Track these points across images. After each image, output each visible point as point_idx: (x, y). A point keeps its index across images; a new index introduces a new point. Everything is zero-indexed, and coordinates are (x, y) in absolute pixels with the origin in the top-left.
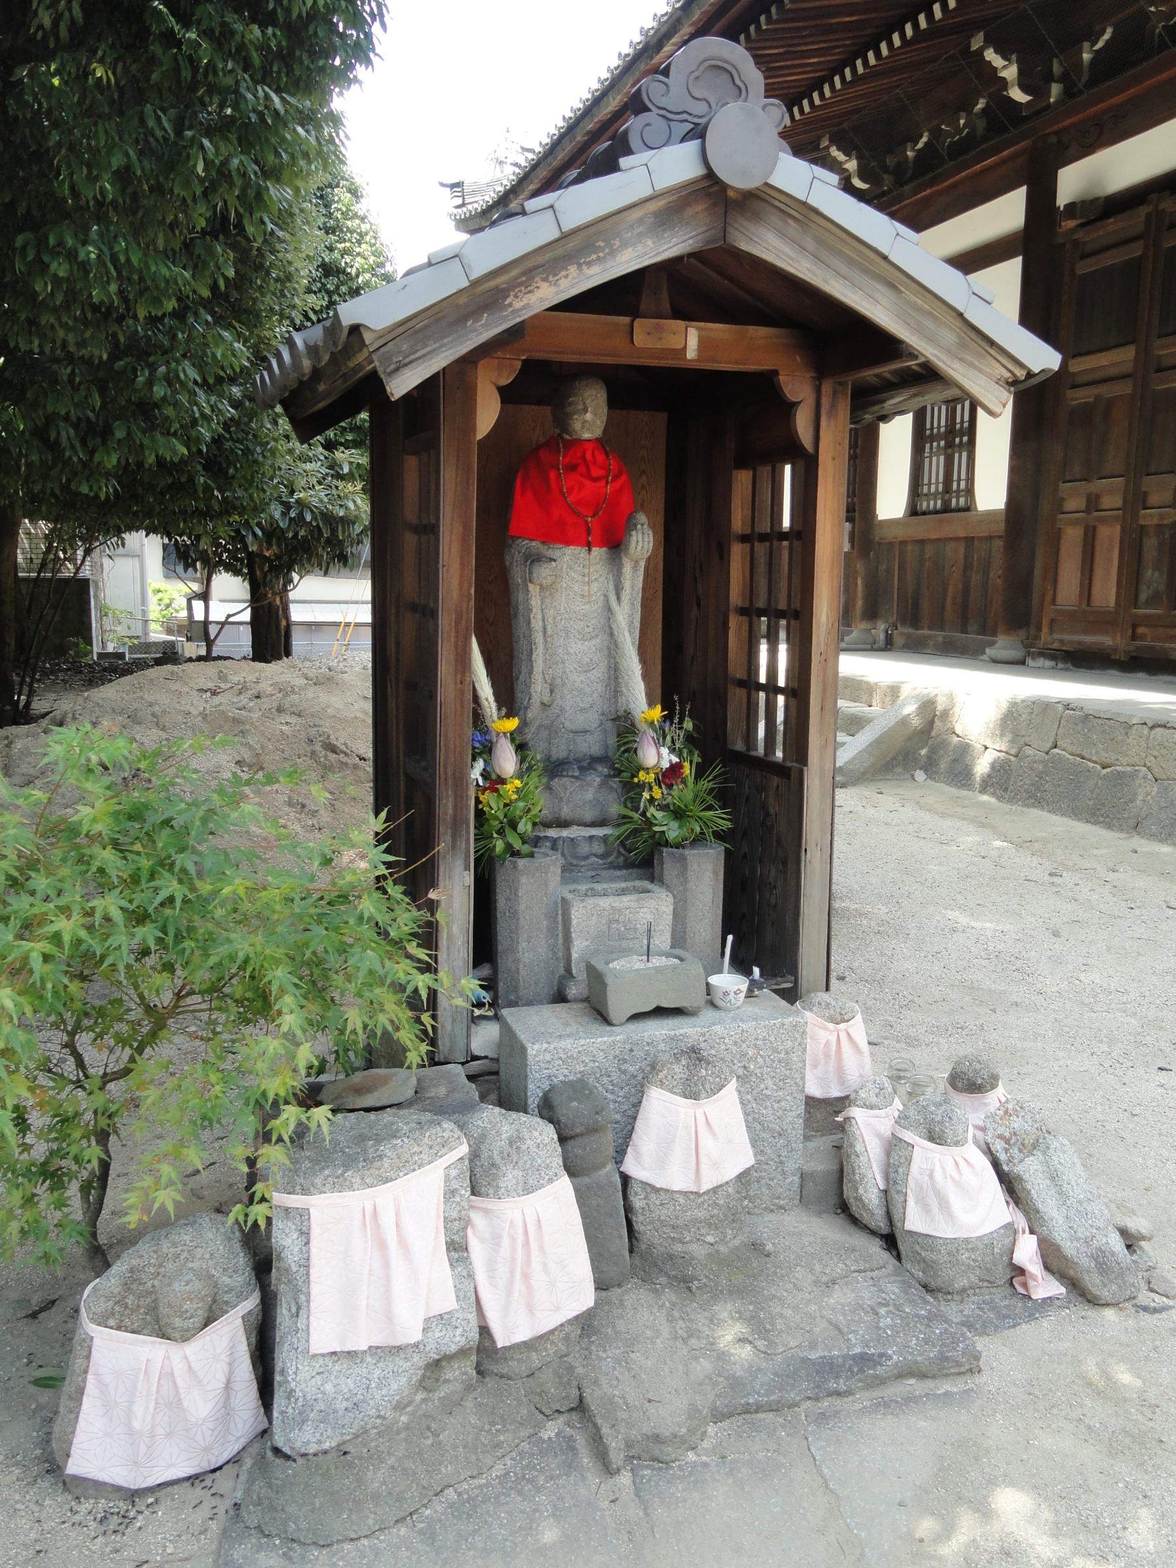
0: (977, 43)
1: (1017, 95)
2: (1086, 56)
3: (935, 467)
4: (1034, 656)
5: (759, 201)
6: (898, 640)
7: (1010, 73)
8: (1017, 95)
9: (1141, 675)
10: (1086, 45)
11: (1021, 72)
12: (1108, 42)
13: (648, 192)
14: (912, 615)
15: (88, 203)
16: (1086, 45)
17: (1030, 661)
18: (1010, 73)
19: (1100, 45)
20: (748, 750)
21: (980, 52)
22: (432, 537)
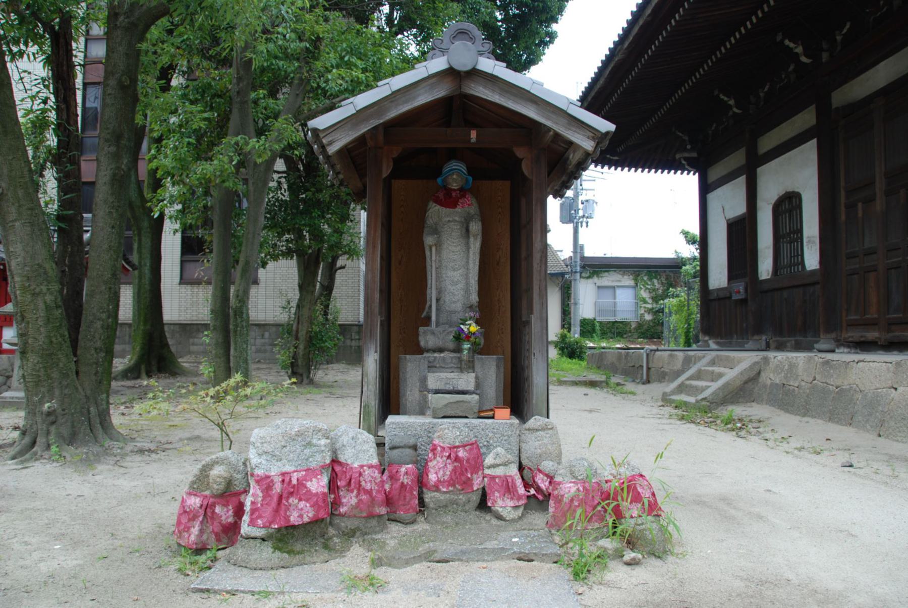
0: (779, 38)
1: (804, 59)
2: (839, 38)
3: (785, 248)
4: (838, 346)
5: (475, 73)
6: (773, 345)
7: (799, 50)
8: (804, 59)
9: (895, 352)
10: (837, 32)
11: (804, 49)
12: (848, 30)
13: (426, 75)
14: (779, 331)
15: (205, 119)
16: (837, 32)
17: (837, 351)
18: (799, 50)
19: (845, 31)
20: (206, 326)
21: (782, 42)
22: (764, 347)
